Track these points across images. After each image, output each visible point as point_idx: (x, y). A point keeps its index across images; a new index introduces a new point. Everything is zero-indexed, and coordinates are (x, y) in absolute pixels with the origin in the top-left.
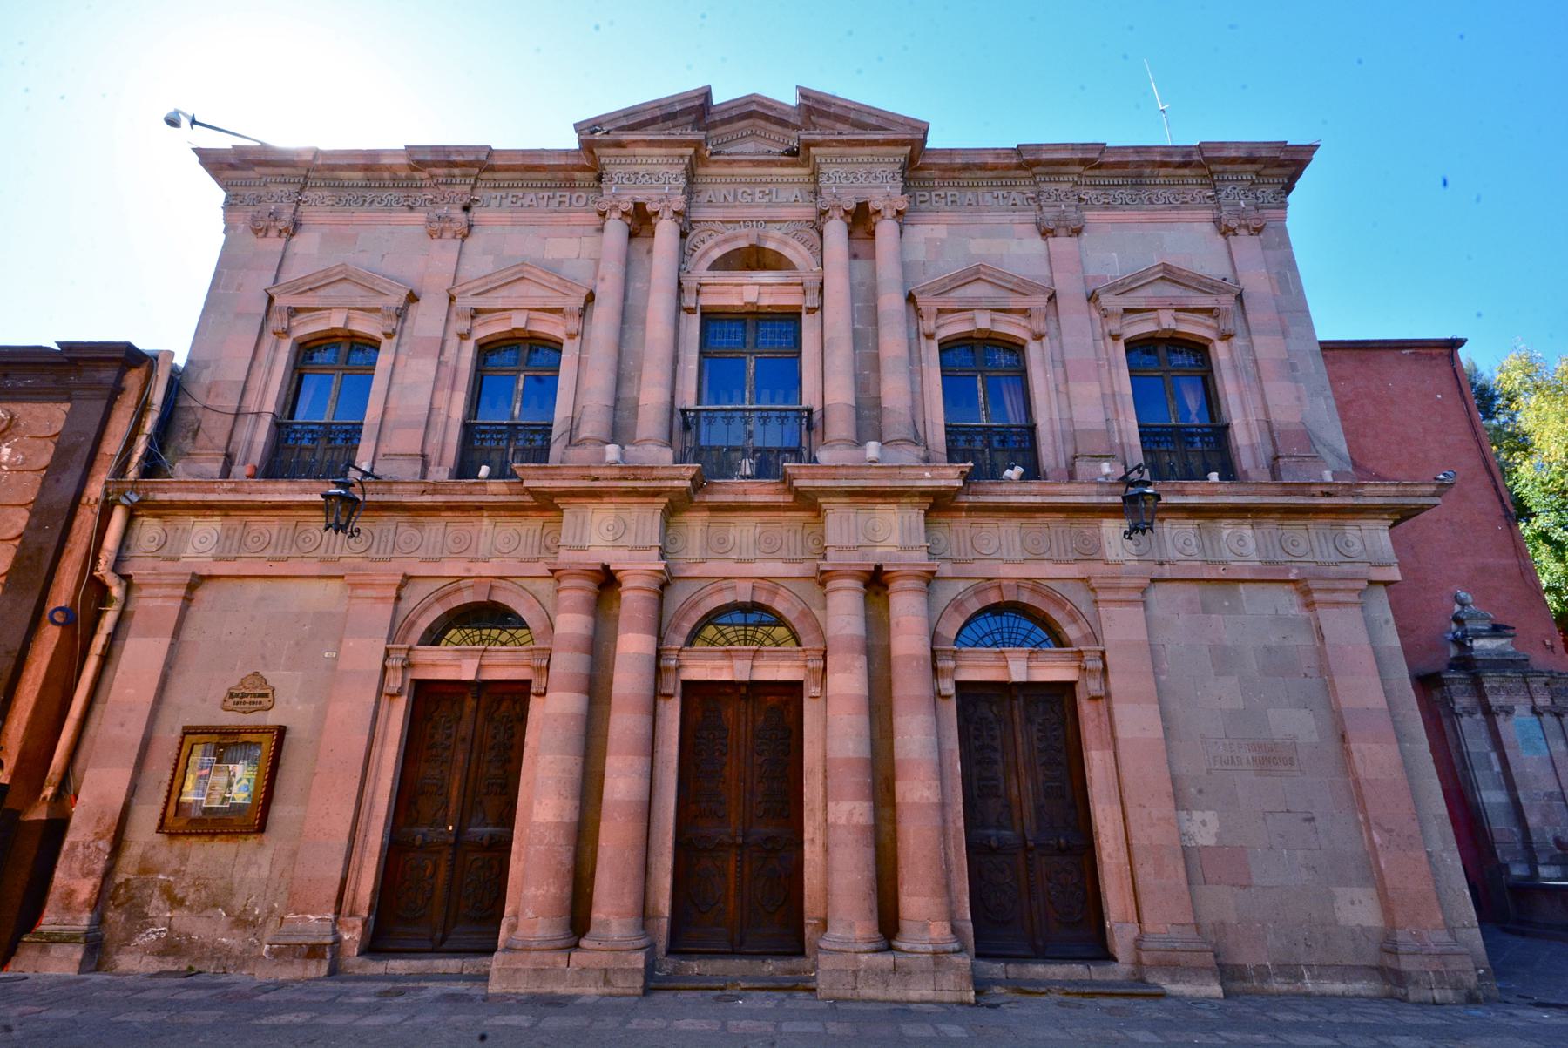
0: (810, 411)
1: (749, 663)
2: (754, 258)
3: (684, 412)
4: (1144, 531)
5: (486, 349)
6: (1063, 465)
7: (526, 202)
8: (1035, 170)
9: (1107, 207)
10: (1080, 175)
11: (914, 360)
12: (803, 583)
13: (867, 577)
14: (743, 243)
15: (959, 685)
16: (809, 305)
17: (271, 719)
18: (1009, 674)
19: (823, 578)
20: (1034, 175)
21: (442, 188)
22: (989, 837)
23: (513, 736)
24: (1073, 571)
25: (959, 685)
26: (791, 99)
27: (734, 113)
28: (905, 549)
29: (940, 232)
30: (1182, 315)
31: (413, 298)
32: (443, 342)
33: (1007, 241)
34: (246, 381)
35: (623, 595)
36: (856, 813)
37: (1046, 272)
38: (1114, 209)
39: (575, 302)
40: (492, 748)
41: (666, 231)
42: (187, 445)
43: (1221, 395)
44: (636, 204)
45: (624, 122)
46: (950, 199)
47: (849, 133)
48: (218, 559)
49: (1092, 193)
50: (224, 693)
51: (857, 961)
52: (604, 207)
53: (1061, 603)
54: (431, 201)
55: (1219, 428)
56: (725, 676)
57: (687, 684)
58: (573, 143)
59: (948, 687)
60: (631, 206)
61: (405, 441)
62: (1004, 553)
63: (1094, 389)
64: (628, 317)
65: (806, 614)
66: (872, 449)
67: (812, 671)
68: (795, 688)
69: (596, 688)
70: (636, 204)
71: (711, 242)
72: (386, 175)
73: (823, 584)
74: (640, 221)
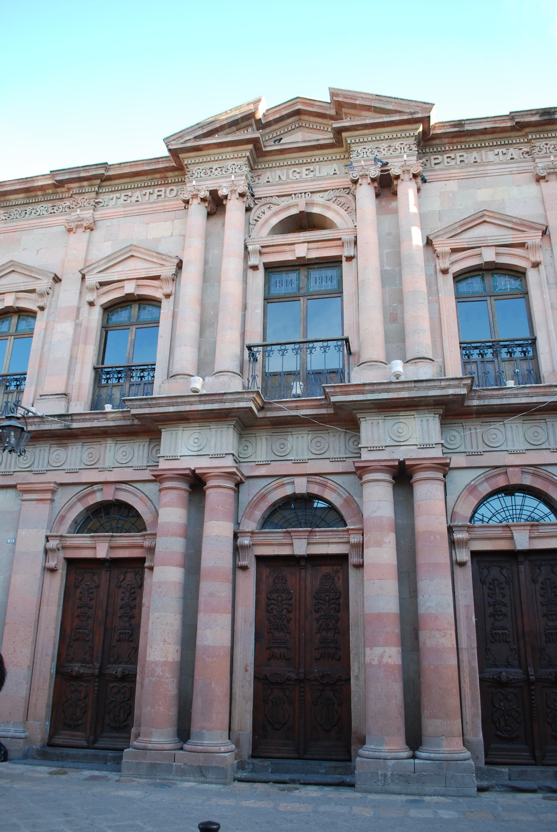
1: (305, 541)
2: (304, 222)
5: (110, 309)
7: (134, 199)
11: (433, 292)
12: (346, 477)
14: (294, 211)
15: (474, 554)
18: (515, 546)
19: (360, 471)
21: (76, 197)
22: (500, 673)
23: (135, 599)
25: (474, 554)
27: (284, 113)
28: (424, 447)
29: (452, 185)
31: (57, 280)
32: (78, 309)
35: (208, 492)
39: (168, 271)
41: (234, 209)
45: (200, 132)
47: (370, 118)
49: (133, 730)
52: (187, 196)
56: (285, 551)
57: (260, 559)
59: (464, 555)
60: (207, 194)
64: (210, 277)
65: (349, 501)
71: (268, 213)
74: (216, 204)
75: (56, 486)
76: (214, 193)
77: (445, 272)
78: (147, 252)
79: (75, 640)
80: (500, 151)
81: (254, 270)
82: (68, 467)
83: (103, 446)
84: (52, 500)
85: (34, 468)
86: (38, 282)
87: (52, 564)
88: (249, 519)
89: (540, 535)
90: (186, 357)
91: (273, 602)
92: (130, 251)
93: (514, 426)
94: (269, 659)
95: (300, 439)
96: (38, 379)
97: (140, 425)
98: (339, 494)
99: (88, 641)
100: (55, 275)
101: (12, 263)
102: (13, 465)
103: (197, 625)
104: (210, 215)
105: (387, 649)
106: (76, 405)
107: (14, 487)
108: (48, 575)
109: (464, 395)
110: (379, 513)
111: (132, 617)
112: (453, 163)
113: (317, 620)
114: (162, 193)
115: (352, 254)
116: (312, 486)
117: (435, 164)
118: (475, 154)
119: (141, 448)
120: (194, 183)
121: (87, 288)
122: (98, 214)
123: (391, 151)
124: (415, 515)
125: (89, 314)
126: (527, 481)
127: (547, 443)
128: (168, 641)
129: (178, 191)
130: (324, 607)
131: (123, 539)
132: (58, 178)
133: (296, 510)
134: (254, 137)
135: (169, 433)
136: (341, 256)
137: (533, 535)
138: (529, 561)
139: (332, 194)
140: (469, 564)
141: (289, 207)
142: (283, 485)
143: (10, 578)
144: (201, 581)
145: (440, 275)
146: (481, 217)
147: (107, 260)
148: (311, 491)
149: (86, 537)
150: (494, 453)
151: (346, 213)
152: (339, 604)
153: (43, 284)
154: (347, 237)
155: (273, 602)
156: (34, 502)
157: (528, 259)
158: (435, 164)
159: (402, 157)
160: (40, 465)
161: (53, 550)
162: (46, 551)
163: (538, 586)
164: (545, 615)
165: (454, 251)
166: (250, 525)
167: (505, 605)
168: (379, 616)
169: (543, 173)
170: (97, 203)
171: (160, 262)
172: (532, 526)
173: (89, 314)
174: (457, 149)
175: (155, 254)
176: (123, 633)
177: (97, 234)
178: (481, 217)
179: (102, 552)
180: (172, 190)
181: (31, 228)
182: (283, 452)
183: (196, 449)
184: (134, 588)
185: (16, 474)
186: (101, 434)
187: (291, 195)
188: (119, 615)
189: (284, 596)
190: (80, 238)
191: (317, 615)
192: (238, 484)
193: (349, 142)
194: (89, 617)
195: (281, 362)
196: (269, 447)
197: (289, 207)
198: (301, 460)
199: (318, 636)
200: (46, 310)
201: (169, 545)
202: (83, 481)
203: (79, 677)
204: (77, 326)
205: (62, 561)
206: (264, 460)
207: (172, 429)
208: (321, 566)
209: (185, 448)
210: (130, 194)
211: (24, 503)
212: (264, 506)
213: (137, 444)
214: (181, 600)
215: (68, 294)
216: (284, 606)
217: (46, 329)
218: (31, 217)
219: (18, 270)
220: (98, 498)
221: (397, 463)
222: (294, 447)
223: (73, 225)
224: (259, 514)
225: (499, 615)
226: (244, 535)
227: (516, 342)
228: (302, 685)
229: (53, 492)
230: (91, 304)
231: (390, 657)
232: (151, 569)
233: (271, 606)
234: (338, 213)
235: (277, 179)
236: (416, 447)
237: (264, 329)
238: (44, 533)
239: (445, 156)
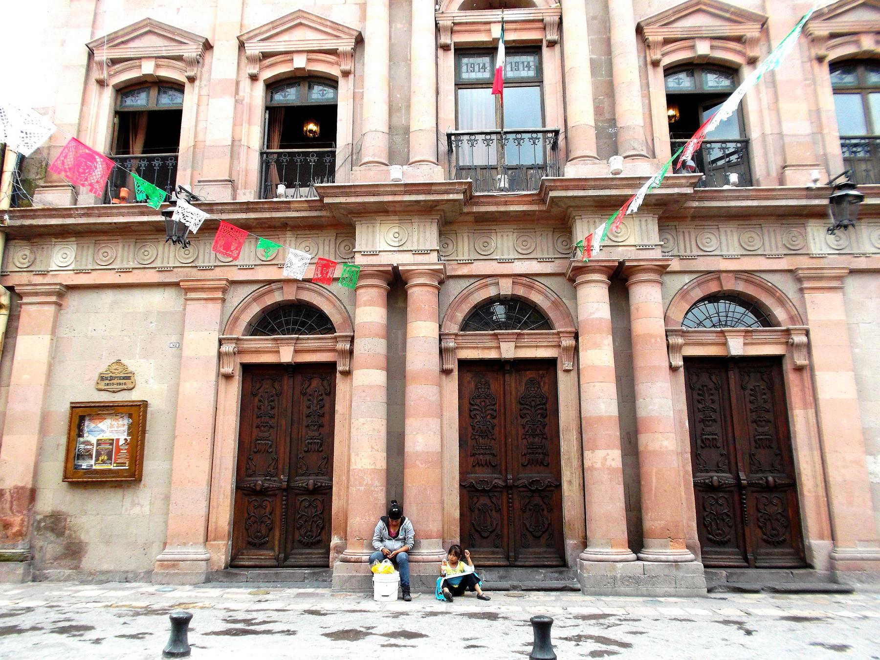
1: (513, 344)
13: (612, 272)
15: (686, 359)
16: (549, 37)
22: (712, 477)
24: (782, 264)
25: (686, 359)
32: (237, 83)
34: (79, 124)
35: (410, 291)
36: (609, 458)
39: (346, 45)
51: (614, 568)
53: (771, 291)
56: (492, 355)
59: (679, 362)
62: (726, 252)
63: (803, 107)
64: (398, 56)
65: (557, 304)
66: (617, 163)
67: (566, 349)
68: (550, 364)
73: (572, 280)
77: (655, 64)
78: (319, 20)
81: (445, 50)
84: (224, 300)
85: (200, 263)
86: (184, 47)
89: (754, 341)
90: (375, 146)
92: (298, 18)
93: (771, 229)
96: (193, 162)
98: (546, 296)
100: (207, 39)
101: (148, 22)
102: (172, 259)
107: (176, 285)
109: (825, 206)
110: (597, 315)
111: (321, 426)
116: (516, 287)
119: (327, 243)
121: (248, 58)
124: (632, 317)
127: (762, 249)
128: (376, 447)
131: (311, 341)
135: (365, 226)
136: (541, 41)
137: (747, 341)
138: (739, 368)
140: (682, 369)
142: (486, 286)
143: (178, 385)
145: (650, 67)
147: (270, 26)
150: (709, 258)
153: (191, 51)
156: (202, 302)
160: (206, 261)
161: (227, 354)
162: (220, 355)
163: (748, 392)
164: (754, 421)
167: (715, 411)
168: (600, 419)
171: (335, 33)
172: (747, 332)
175: (329, 23)
176: (311, 443)
179: (286, 355)
185: (175, 270)
186: (279, 227)
188: (305, 423)
191: (524, 421)
192: (441, 283)
194: (271, 427)
195: (479, 155)
196: (472, 246)
198: (509, 261)
199: (525, 441)
200: (197, 83)
201: (370, 347)
203: (263, 492)
205: (238, 367)
206: (467, 258)
207: (482, 228)
208: (526, 370)
211: (189, 302)
212: (466, 308)
213: (322, 239)
215: (224, 63)
219: (156, 31)
220: (278, 297)
221: (390, 268)
224: (460, 316)
225: (708, 421)
228: (510, 492)
229: (224, 290)
230: (254, 78)
231: (613, 460)
232: (347, 373)
233: (475, 412)
236: (634, 248)
238: (215, 336)
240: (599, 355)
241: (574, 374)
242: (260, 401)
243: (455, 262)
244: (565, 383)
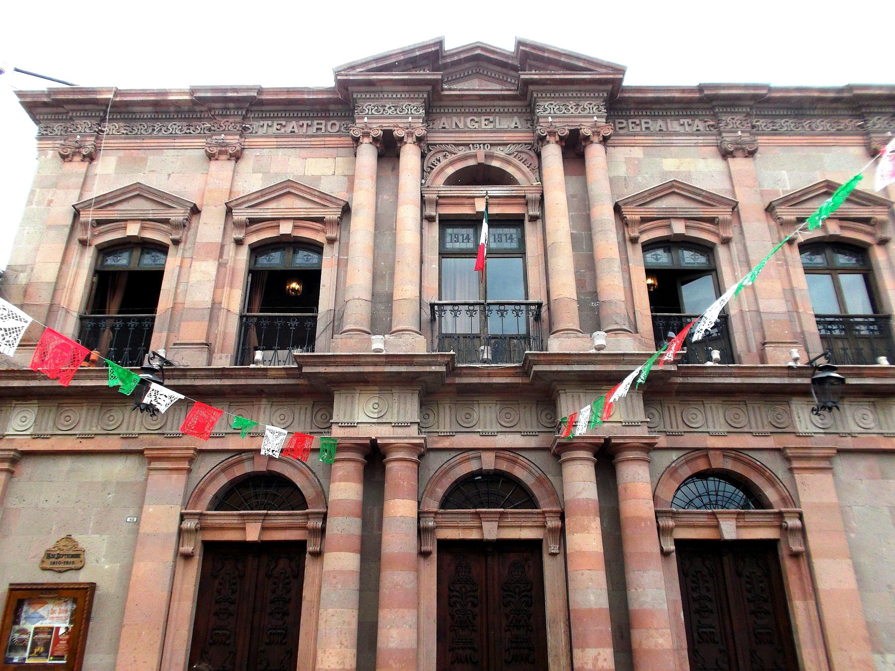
0: (539, 305)
1: (496, 524)
3: (432, 306)
4: (830, 409)
6: (754, 350)
7: (289, 129)
8: (714, 103)
9: (775, 132)
10: (751, 108)
12: (544, 455)
13: (597, 449)
14: (471, 162)
15: (678, 542)
17: (82, 577)
20: (713, 108)
24: (769, 442)
25: (678, 542)
26: (509, 47)
29: (638, 152)
30: (845, 224)
32: (222, 247)
33: (696, 164)
36: (601, 658)
37: (727, 185)
38: (781, 134)
39: (332, 214)
40: (272, 602)
42: (504, 411)
43: (881, 289)
44: (384, 131)
46: (644, 126)
48: (36, 437)
49: (761, 123)
50: (42, 554)
52: (357, 133)
53: (760, 470)
54: (210, 130)
55: (881, 318)
56: (474, 535)
58: (331, 83)
60: (381, 133)
61: (193, 331)
64: (385, 225)
65: (542, 481)
66: (600, 338)
67: (552, 531)
68: (535, 546)
69: (370, 550)
70: (384, 131)
71: (444, 162)
72: (172, 109)
73: (557, 456)
74: (388, 148)
75: (17, 455)
76: (388, 134)
77: (634, 241)
79: (210, 644)
80: (686, 121)
81: (429, 221)
82: (124, 431)
83: (256, 407)
84: (189, 471)
85: (167, 431)
87: (187, 548)
88: (431, 497)
89: (746, 524)
91: (509, 593)
92: (287, 187)
93: (756, 406)
94: (453, 663)
95: (488, 409)
97: (306, 385)
99: (228, 645)
101: (138, 186)
102: (138, 425)
103: (377, 623)
104: (380, 157)
105: (601, 650)
106: (221, 358)
107: (140, 453)
108: (181, 562)
110: (584, 495)
112: (638, 129)
113: (507, 617)
114: (323, 127)
115: (538, 213)
116: (500, 461)
117: (620, 128)
118: (660, 122)
119: (303, 411)
120: (366, 120)
121: (234, 223)
122: (249, 141)
123: (579, 110)
124: (620, 498)
125: (236, 254)
126: (729, 465)
128: (345, 643)
129: (340, 127)
130: (513, 600)
132: (198, 95)
133: (490, 488)
134: (432, 79)
137: (739, 524)
139: (512, 148)
141: (465, 158)
143: (132, 564)
144: (383, 568)
146: (671, 187)
148: (498, 467)
149: (234, 515)
150: (695, 434)
151: (528, 169)
152: (531, 597)
153: (178, 215)
154: (533, 195)
155: (455, 593)
157: (717, 235)
158: (620, 128)
159: (589, 117)
161: (189, 531)
162: (181, 532)
164: (753, 613)
165: (644, 220)
166: (433, 505)
169: (730, 148)
170: (245, 129)
173: (236, 254)
174: (642, 115)
176: (274, 634)
177: (246, 165)
178: (671, 187)
179: (253, 533)
180: (334, 124)
181: (160, 149)
182: (469, 423)
183: (376, 416)
184: (288, 578)
185: (141, 437)
187: (468, 145)
189: (468, 587)
190: (222, 169)
192: (421, 456)
193: (535, 95)
195: (460, 324)
197: (465, 158)
198: (492, 435)
200: (181, 246)
201: (343, 526)
202: (230, 448)
204: (221, 266)
205: (200, 544)
209: (363, 417)
210: (284, 123)
212: (447, 483)
213: (298, 406)
214: (358, 593)
215: (210, 228)
216: (469, 599)
217: (181, 267)
218: (160, 134)
221: (368, 442)
222: (481, 418)
223: (215, 150)
224: (440, 492)
225: (704, 612)
226: (426, 515)
227: (828, 319)
229: (191, 460)
231: (605, 660)
233: (454, 599)
234: (519, 169)
235: (454, 126)
236: (620, 424)
237: (440, 286)
238: (177, 510)
239: (630, 121)
240: (587, 539)
241: (560, 558)
242: (220, 584)
243: (436, 434)
244: (551, 568)
